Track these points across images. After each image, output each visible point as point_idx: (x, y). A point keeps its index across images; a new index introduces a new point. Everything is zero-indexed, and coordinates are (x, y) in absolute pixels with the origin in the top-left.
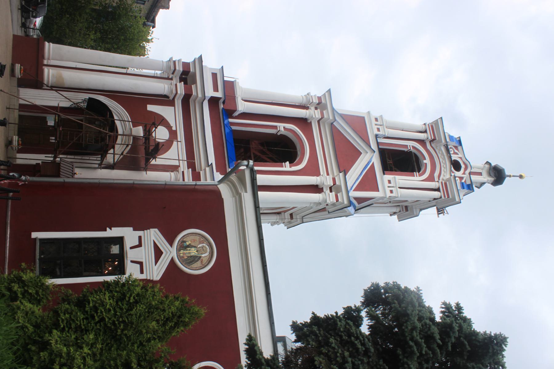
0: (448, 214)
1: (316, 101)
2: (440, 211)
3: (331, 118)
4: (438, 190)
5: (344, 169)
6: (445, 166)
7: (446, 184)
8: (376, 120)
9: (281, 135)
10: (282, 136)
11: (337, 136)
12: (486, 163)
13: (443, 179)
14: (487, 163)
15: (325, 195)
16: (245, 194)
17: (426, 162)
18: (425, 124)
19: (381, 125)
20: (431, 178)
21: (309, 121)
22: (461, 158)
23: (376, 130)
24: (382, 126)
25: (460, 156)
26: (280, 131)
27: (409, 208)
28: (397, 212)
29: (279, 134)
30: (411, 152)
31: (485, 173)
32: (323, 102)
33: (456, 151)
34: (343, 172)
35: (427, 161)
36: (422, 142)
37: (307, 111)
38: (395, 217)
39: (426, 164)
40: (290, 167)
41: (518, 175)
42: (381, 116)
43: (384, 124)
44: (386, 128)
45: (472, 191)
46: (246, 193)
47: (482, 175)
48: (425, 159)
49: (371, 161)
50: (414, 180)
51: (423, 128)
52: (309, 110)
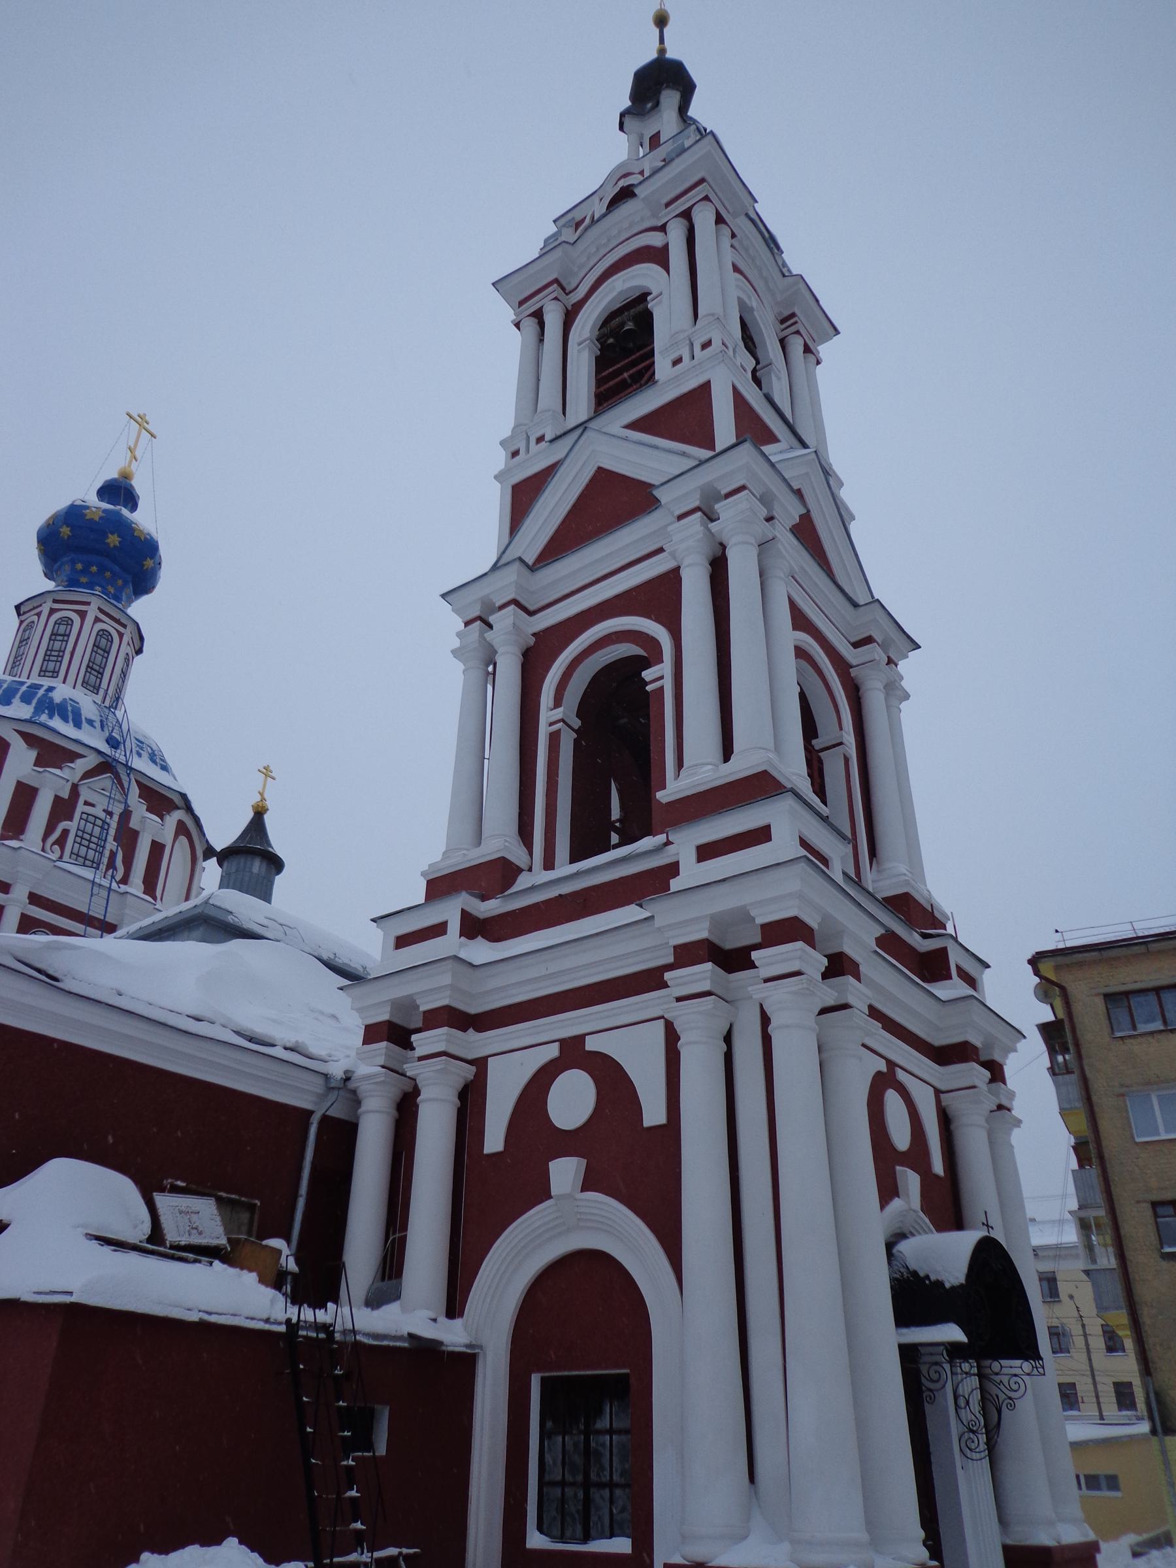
8: (515, 454)
9: (579, 715)
10: (583, 710)
19: (528, 438)
20: (660, 257)
27: (786, 313)
28: (803, 343)
29: (577, 723)
37: (499, 652)
38: (823, 350)
41: (657, 31)
51: (530, 325)
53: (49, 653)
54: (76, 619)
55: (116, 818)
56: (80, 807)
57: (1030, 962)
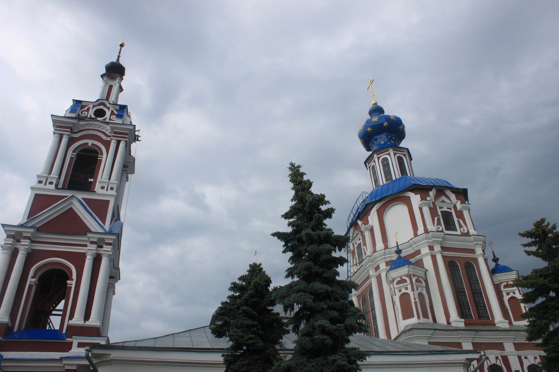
0: (139, 130)
1: (11, 241)
2: (136, 138)
3: (32, 230)
4: (118, 142)
5: (84, 230)
6: (98, 126)
7: (115, 133)
8: (40, 182)
11: (49, 228)
12: (102, 78)
13: (110, 133)
14: (102, 76)
15: (104, 255)
16: (112, 356)
17: (91, 144)
18: (54, 133)
19: (47, 179)
21: (30, 251)
22: (94, 106)
23: (51, 185)
24: (48, 178)
25: (91, 106)
26: (36, 282)
27: (126, 164)
30: (78, 154)
31: (111, 83)
32: (13, 234)
33: (86, 109)
34: (87, 233)
35: (90, 142)
36: (71, 141)
39: (92, 144)
40: (72, 280)
42: (38, 176)
43: (46, 175)
44: (50, 174)
45: (126, 107)
46: (111, 355)
47: (113, 86)
48: (88, 143)
49: (80, 200)
50: (106, 160)
51: (57, 137)
52: (20, 249)
53: (390, 173)
54: (388, 156)
55: (453, 209)
56: (439, 211)
57: (135, 125)
